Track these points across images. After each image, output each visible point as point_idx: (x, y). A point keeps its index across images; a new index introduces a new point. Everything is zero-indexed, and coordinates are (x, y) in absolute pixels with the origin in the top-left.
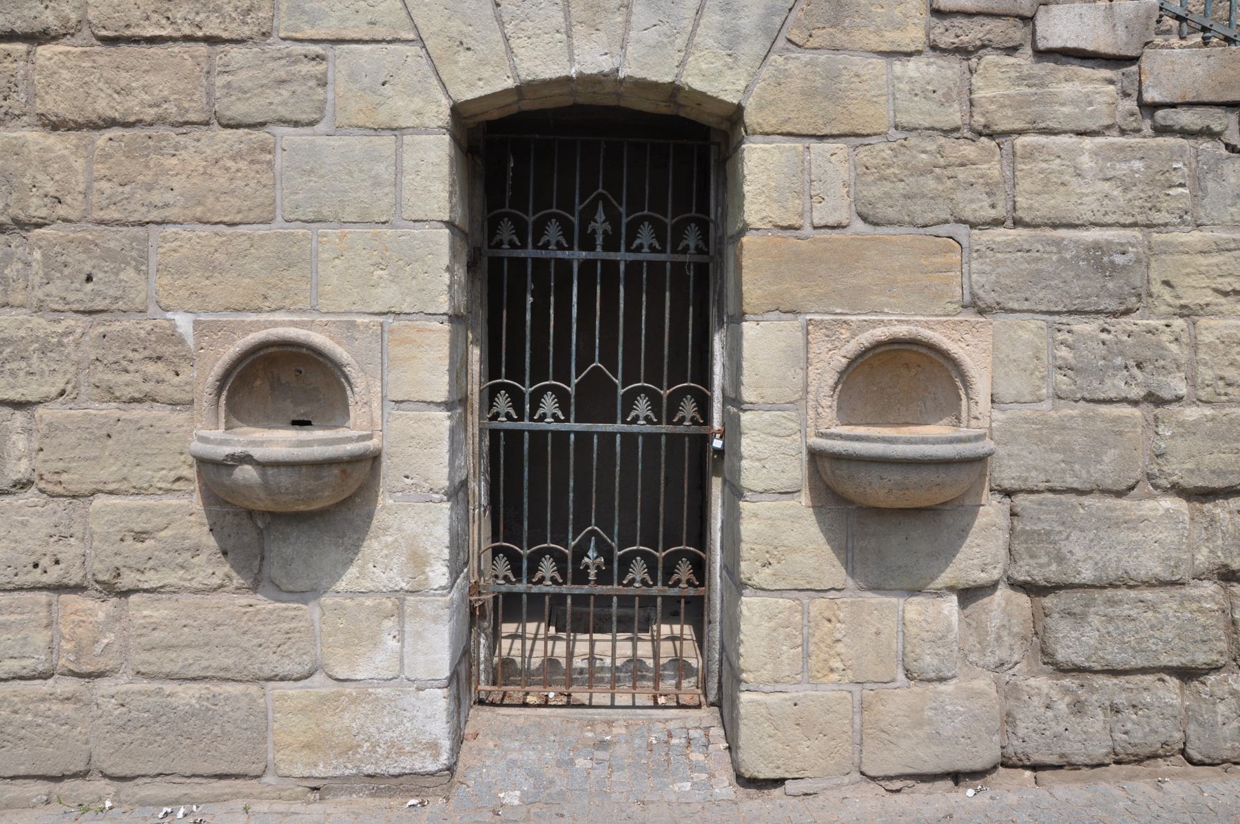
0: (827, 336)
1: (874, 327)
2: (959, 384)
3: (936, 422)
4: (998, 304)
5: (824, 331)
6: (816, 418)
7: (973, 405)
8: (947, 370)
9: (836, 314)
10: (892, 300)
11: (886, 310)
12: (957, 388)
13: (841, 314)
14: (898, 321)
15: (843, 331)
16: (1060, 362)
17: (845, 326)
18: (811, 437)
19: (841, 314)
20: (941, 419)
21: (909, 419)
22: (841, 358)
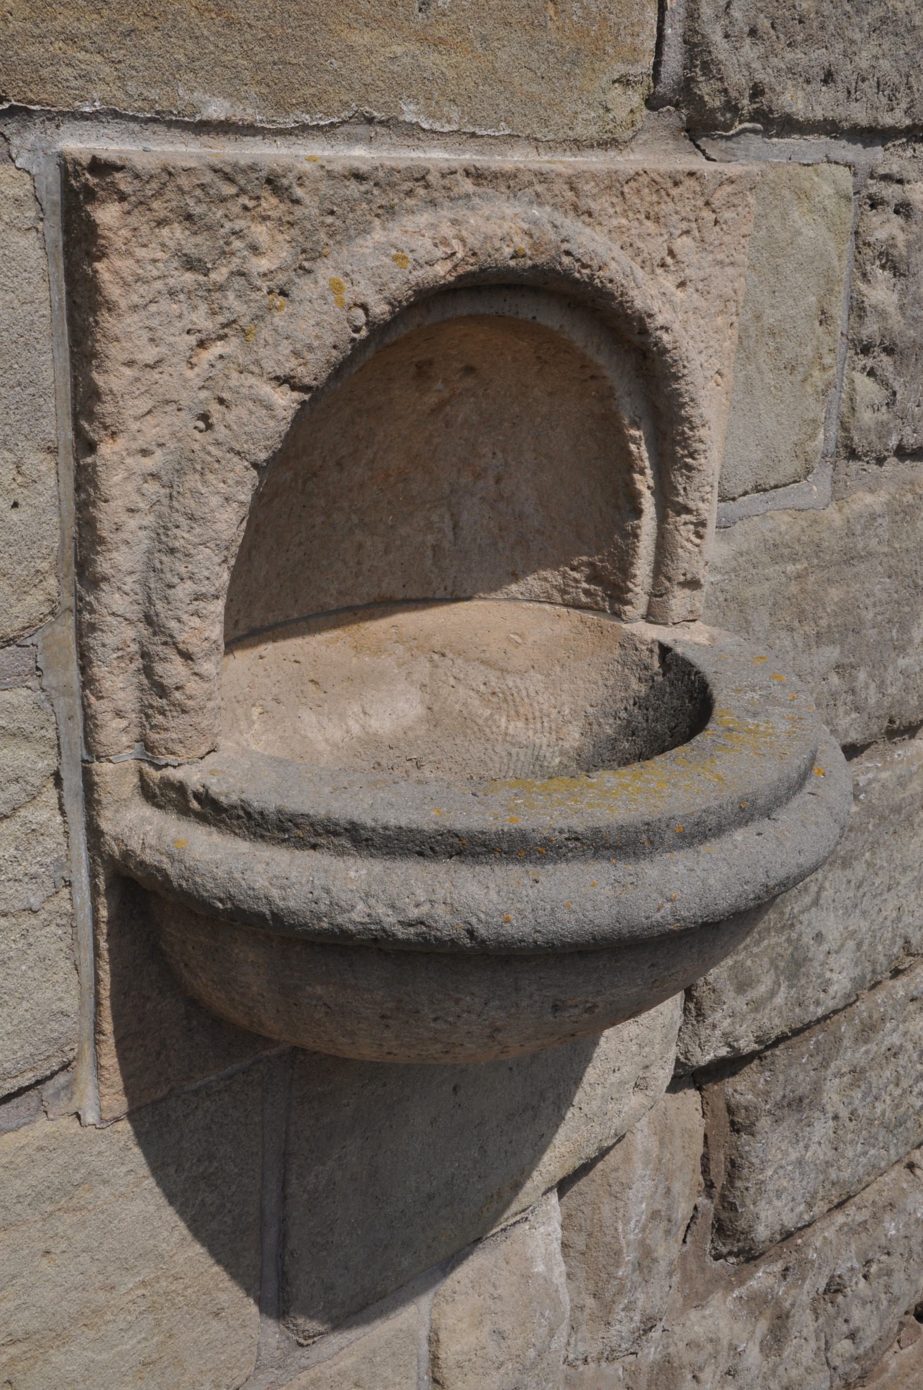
0: (191, 264)
1: (390, 211)
2: (641, 452)
3: (493, 586)
4: (757, 91)
5: (176, 234)
6: (145, 711)
7: (683, 531)
8: (607, 396)
9: (204, 127)
10: (433, 60)
11: (409, 113)
12: (629, 465)
13: (225, 128)
14: (477, 175)
15: (260, 232)
16: (871, 329)
17: (270, 203)
18: (123, 803)
19: (225, 128)
20: (515, 577)
21: (392, 586)
22: (267, 390)
